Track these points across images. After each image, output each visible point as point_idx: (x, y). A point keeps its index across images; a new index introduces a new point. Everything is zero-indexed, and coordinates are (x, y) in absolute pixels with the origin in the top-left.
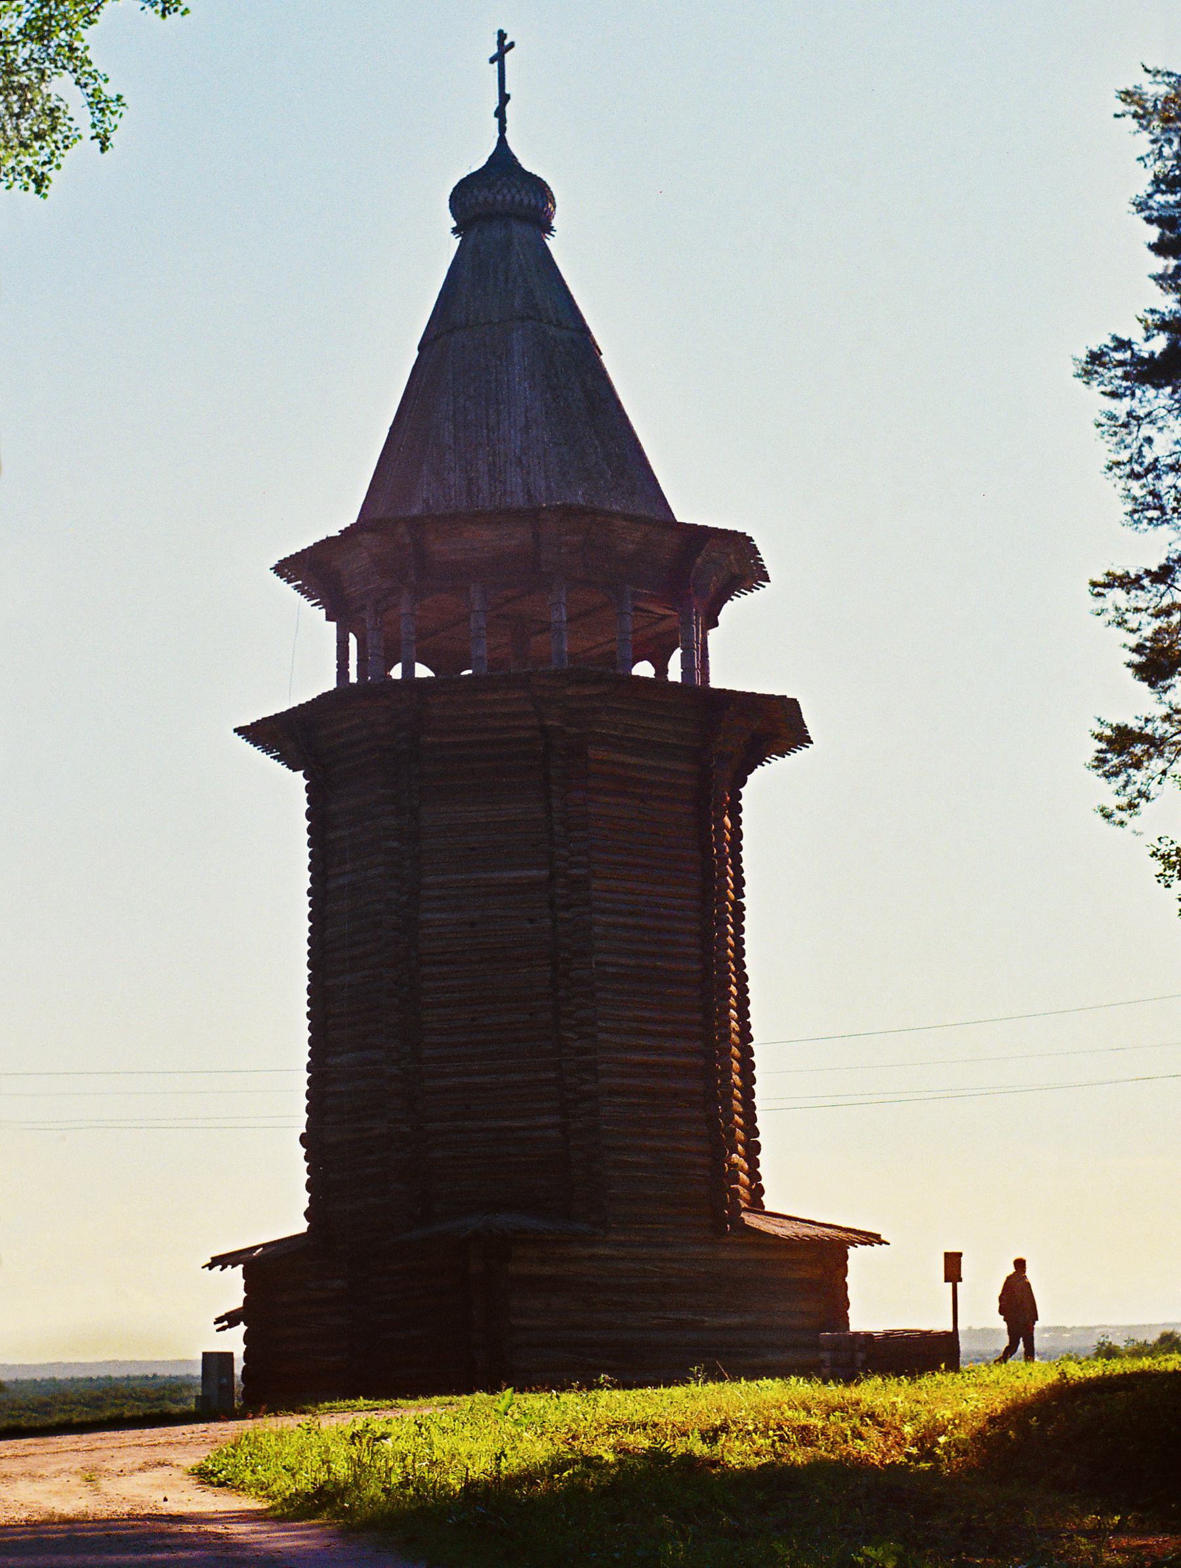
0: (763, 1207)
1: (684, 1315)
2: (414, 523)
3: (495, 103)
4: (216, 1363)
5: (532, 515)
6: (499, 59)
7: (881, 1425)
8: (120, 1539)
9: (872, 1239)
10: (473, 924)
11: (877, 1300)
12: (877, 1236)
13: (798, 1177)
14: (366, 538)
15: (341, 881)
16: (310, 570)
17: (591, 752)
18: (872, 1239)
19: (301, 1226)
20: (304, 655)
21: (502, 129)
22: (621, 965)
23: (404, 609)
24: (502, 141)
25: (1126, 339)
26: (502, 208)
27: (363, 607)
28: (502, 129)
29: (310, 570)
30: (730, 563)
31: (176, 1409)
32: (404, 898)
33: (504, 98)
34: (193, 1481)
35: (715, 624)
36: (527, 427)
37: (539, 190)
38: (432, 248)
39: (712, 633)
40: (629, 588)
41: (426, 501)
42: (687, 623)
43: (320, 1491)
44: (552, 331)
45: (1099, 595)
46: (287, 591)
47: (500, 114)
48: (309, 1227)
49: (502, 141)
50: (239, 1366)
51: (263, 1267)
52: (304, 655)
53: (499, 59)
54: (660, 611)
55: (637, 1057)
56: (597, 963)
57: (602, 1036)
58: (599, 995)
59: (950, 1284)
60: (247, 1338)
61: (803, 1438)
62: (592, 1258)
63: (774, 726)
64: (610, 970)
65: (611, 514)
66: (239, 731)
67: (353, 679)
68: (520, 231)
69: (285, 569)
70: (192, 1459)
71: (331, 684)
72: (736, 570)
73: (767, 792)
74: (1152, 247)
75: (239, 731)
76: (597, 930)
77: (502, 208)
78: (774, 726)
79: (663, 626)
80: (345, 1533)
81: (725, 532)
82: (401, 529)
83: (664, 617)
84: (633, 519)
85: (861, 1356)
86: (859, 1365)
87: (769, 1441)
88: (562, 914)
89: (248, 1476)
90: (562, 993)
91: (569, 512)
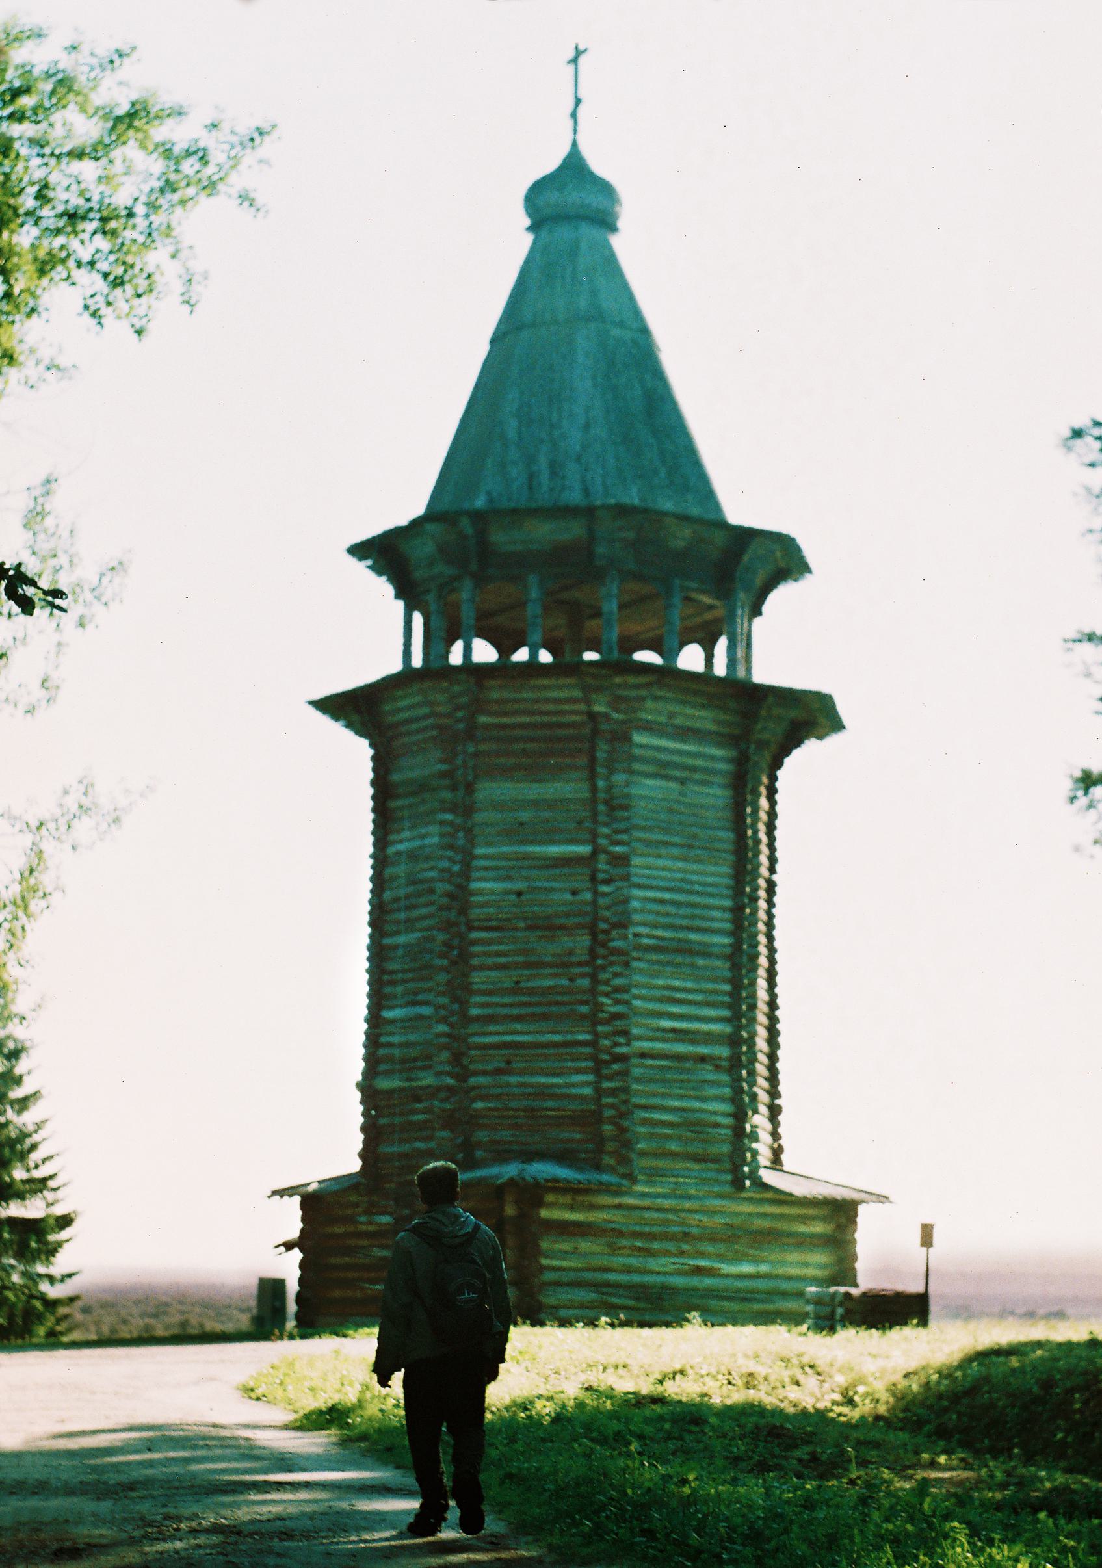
0: (782, 1165)
1: (702, 1263)
2: (477, 516)
4: (272, 1289)
5: (589, 512)
7: (819, 1374)
8: (172, 1439)
9: (883, 1199)
10: (519, 894)
11: (882, 1254)
12: (887, 1198)
13: (813, 1141)
14: (429, 527)
15: (401, 847)
16: (384, 553)
17: (639, 738)
18: (883, 1199)
19: (356, 1165)
20: (375, 635)
21: (575, 132)
22: (657, 938)
23: (465, 595)
24: (574, 143)
26: (570, 208)
27: (428, 591)
28: (575, 132)
29: (384, 553)
32: (456, 868)
34: (239, 1394)
35: (759, 613)
36: (587, 427)
37: (606, 190)
39: (757, 622)
40: (677, 581)
41: (489, 493)
42: (732, 615)
43: (332, 1409)
44: (616, 332)
45: (1069, 650)
46: (361, 570)
48: (363, 1168)
49: (574, 143)
50: (293, 1287)
51: (318, 1204)
52: (375, 635)
53: (575, 61)
54: (708, 600)
55: (667, 1024)
56: (636, 935)
57: (636, 1003)
58: (635, 964)
59: (925, 1249)
60: (302, 1265)
61: (747, 1383)
62: (619, 1206)
64: (646, 941)
65: (665, 514)
68: (588, 232)
69: (359, 550)
70: (242, 1375)
71: (395, 666)
72: (783, 564)
76: (635, 904)
77: (570, 208)
79: (708, 616)
80: (344, 1442)
81: (772, 533)
82: (465, 522)
83: (711, 607)
84: (685, 518)
85: (840, 1311)
86: (838, 1317)
87: (719, 1384)
88: (605, 889)
89: (279, 1393)
90: (599, 962)
91: (622, 511)
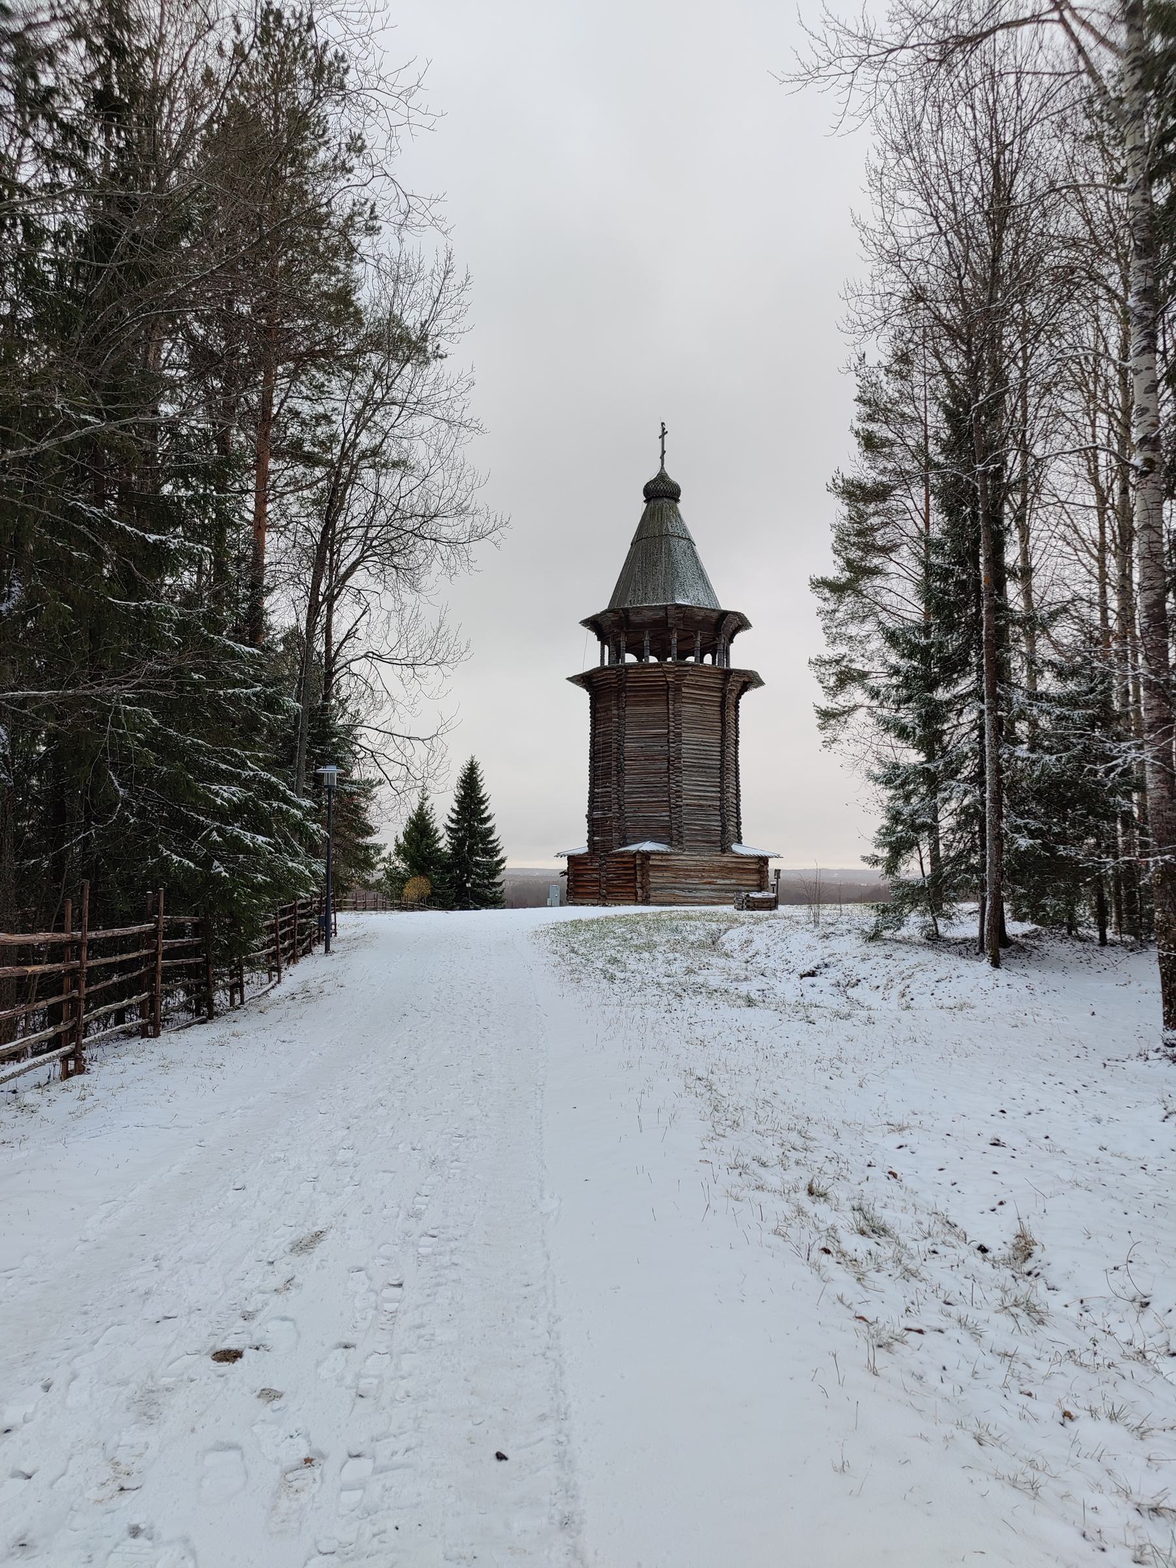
3: (660, 454)
6: (662, 437)
16: (593, 623)
24: (662, 468)
25: (583, 697)
29: (593, 623)
30: (585, 680)
31: (1073, 46)
33: (664, 452)
38: (638, 506)
47: (662, 458)
49: (662, 468)
52: (590, 654)
53: (662, 437)
63: (750, 680)
66: (568, 679)
67: (606, 663)
73: (748, 701)
74: (741, 623)
75: (568, 679)
78: (750, 680)
